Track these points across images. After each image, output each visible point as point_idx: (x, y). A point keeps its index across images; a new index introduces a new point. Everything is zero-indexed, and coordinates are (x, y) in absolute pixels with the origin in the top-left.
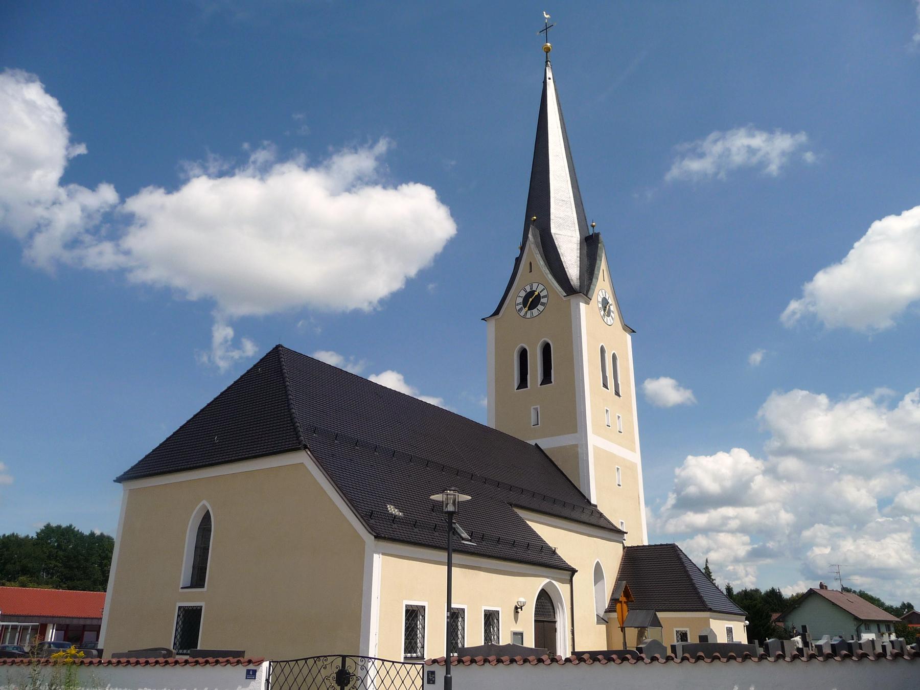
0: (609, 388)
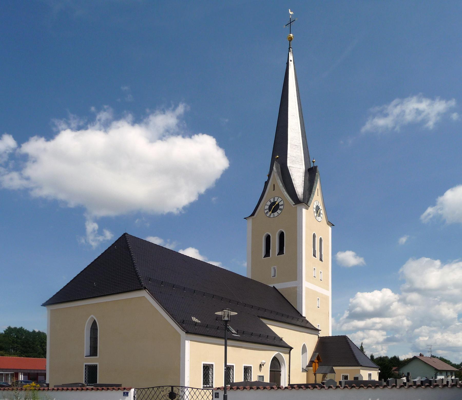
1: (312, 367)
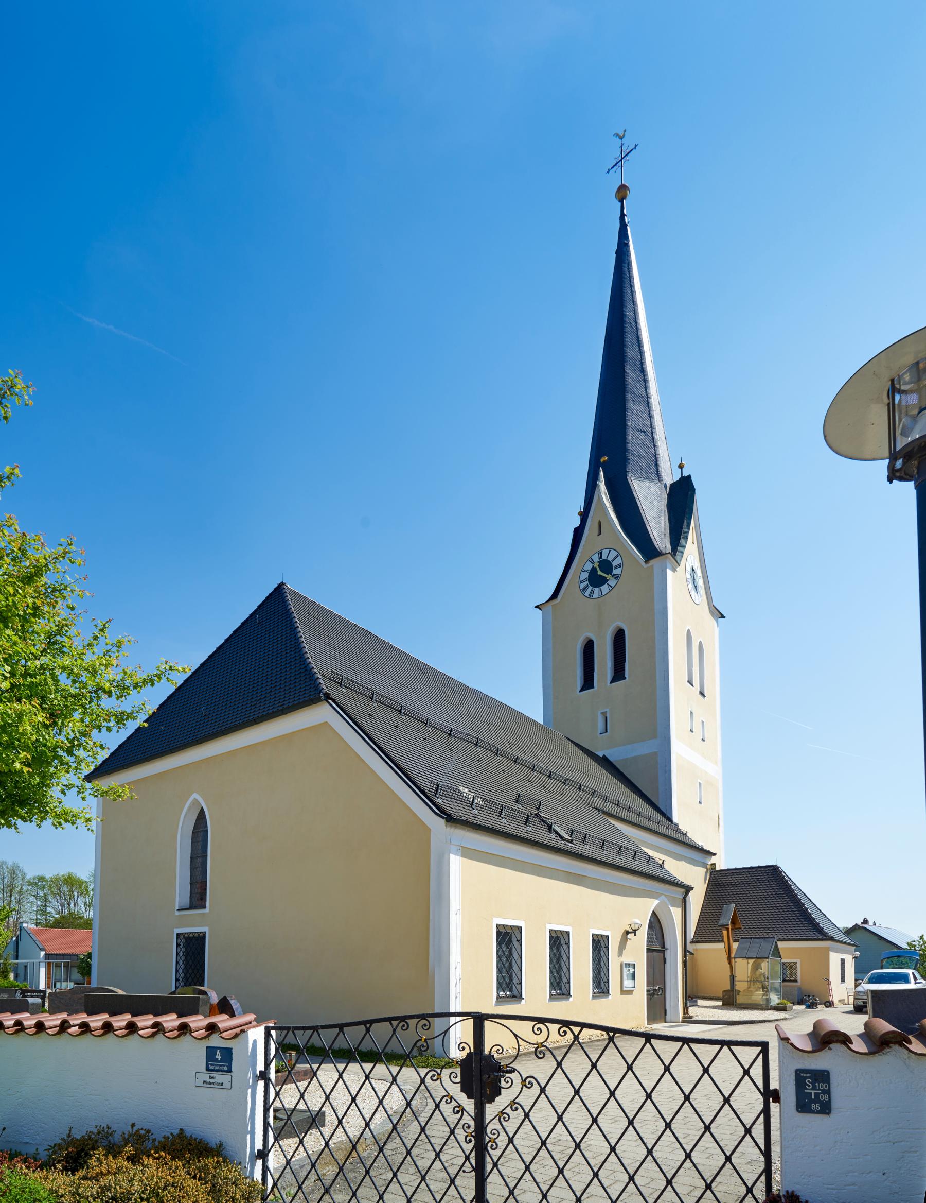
0: (694, 685)
1: (723, 944)
